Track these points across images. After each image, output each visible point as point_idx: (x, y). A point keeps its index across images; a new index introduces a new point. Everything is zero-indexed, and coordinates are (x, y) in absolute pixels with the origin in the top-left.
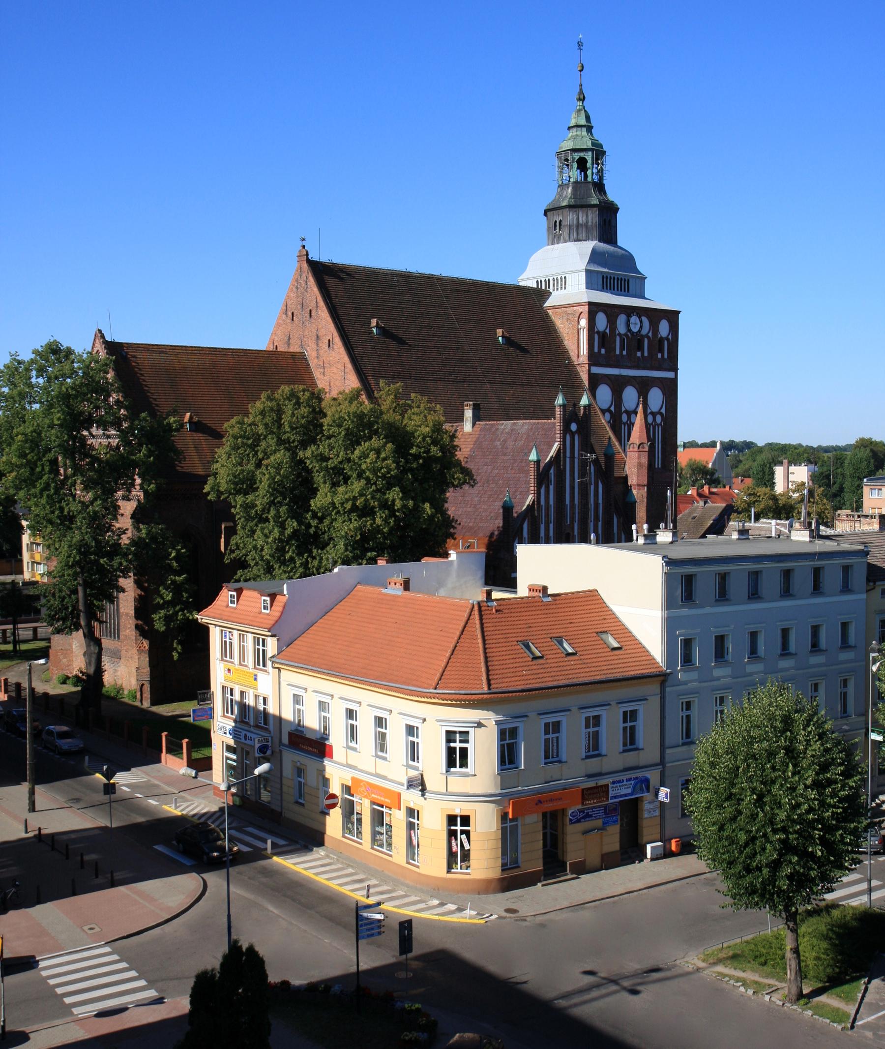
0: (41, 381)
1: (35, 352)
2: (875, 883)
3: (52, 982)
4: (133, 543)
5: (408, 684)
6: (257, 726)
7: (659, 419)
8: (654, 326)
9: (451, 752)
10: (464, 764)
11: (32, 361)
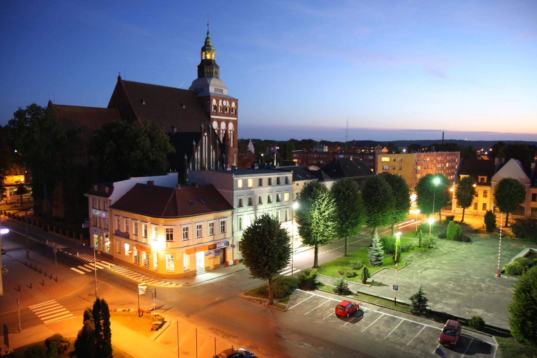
0: (29, 117)
1: (27, 107)
2: (294, 269)
3: (37, 313)
4: (5, 190)
5: (412, 323)
6: (105, 229)
7: (232, 132)
8: (230, 104)
9: (168, 235)
10: (172, 239)
11: (26, 110)
